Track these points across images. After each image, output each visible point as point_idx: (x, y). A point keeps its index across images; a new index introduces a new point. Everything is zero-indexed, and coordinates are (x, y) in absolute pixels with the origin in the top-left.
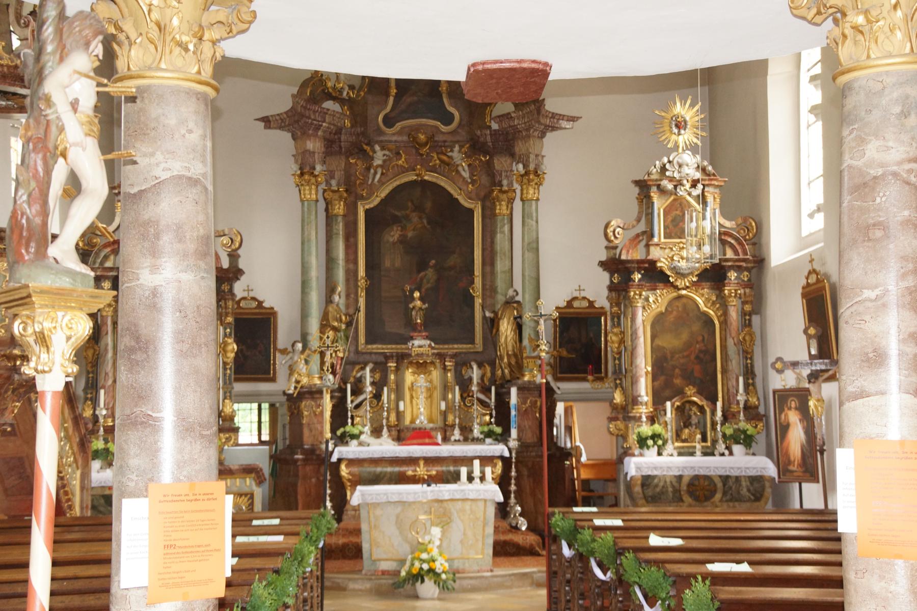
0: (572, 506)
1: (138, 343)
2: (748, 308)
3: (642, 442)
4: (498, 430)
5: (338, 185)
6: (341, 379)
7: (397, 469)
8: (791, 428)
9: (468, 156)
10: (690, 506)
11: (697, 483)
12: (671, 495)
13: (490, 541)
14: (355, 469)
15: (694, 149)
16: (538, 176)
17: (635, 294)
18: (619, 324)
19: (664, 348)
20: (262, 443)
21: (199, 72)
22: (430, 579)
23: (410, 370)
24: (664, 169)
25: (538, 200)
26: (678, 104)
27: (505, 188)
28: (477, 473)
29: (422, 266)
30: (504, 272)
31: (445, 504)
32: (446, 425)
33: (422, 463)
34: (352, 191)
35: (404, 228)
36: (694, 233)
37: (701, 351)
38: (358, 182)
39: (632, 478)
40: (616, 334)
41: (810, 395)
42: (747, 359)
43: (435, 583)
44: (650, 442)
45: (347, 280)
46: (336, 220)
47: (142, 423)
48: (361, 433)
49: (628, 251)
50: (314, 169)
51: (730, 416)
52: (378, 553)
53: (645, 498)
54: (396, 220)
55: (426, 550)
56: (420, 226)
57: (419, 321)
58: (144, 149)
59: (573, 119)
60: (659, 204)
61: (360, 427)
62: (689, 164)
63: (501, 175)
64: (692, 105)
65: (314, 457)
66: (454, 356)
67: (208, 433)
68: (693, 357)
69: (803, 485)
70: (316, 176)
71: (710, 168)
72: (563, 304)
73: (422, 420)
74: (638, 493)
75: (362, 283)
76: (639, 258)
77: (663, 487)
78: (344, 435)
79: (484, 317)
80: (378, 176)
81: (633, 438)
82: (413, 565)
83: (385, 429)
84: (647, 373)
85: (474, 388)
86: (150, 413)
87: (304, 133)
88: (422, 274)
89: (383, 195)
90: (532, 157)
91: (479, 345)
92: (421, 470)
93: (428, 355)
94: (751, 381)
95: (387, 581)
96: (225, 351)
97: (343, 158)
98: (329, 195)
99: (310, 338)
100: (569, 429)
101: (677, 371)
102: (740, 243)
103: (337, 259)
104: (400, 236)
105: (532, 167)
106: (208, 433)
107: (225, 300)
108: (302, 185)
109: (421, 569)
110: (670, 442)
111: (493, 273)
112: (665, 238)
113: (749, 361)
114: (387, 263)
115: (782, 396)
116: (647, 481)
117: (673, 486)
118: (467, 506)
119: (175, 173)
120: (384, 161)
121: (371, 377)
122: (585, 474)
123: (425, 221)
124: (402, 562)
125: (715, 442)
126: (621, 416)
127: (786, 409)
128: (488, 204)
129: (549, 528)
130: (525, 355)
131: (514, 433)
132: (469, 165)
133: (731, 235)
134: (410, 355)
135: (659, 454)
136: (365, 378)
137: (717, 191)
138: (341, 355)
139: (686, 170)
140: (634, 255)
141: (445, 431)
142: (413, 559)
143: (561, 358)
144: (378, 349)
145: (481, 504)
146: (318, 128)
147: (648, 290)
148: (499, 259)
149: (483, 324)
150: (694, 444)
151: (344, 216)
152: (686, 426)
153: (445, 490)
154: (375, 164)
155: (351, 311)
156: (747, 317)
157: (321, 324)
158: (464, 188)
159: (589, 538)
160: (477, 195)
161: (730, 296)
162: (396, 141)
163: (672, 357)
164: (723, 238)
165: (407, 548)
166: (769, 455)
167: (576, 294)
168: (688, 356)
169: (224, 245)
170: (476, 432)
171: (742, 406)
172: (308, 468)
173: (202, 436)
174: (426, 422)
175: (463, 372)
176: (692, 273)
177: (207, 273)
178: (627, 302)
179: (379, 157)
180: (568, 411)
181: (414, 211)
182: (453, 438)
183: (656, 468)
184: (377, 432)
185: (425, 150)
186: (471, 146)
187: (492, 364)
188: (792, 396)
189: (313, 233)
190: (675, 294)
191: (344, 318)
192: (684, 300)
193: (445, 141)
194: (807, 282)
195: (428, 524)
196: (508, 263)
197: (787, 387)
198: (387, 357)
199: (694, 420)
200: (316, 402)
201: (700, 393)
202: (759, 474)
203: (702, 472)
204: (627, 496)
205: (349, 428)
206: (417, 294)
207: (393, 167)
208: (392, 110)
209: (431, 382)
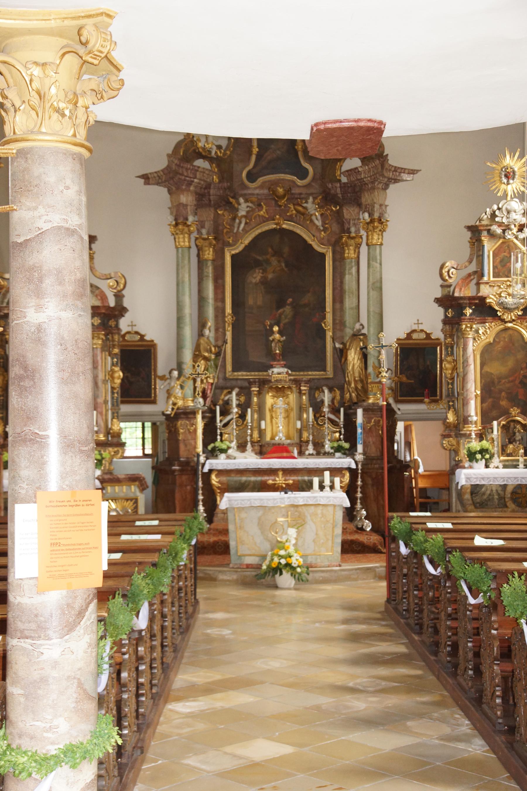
1: (26, 372)
3: (472, 456)
4: (347, 445)
5: (208, 234)
6: (212, 401)
7: (259, 478)
9: (321, 207)
10: (513, 511)
11: (519, 491)
13: (339, 540)
14: (224, 479)
16: (382, 223)
17: (467, 327)
18: (452, 354)
19: (492, 374)
20: (145, 456)
21: (74, 135)
22: (288, 572)
23: (270, 394)
24: (493, 215)
25: (381, 244)
27: (353, 235)
28: (327, 482)
29: (280, 304)
30: (352, 308)
31: (300, 509)
32: (301, 441)
33: (280, 473)
34: (220, 238)
35: (264, 271)
38: (225, 231)
39: (462, 486)
40: (449, 362)
43: (292, 575)
45: (216, 317)
46: (207, 264)
47: (31, 440)
48: (229, 448)
49: (461, 289)
50: (187, 219)
52: (243, 550)
53: (474, 504)
54: (258, 264)
55: (283, 548)
56: (279, 268)
57: (278, 352)
58: (28, 204)
59: (413, 172)
60: (489, 247)
61: (227, 443)
63: (349, 223)
65: (189, 468)
66: (308, 382)
67: (86, 448)
68: (517, 382)
70: (189, 226)
72: (403, 336)
73: (281, 437)
74: (468, 500)
75: (229, 319)
76: (470, 295)
77: (490, 495)
78: (214, 450)
79: (335, 348)
80: (242, 226)
81: (463, 452)
82: (272, 560)
83: (249, 445)
84: (476, 396)
85: (326, 410)
86: (37, 431)
87: (178, 189)
88: (281, 311)
89: (247, 242)
90: (377, 207)
91: (330, 372)
92: (280, 480)
93: (285, 381)
95: (251, 573)
96: (113, 377)
97: (212, 210)
98: (200, 243)
99: (184, 366)
100: (408, 444)
103: (208, 298)
104: (262, 277)
105: (376, 216)
106: (86, 448)
107: (112, 334)
108: (177, 234)
109: (280, 563)
110: (496, 456)
111: (342, 309)
112: (494, 277)
114: (251, 301)
116: (475, 489)
117: (499, 494)
118: (319, 510)
119: (55, 224)
120: (248, 212)
121: (237, 400)
122: (422, 484)
123: (283, 265)
124: (264, 557)
126: (453, 434)
128: (338, 249)
129: (389, 529)
130: (369, 381)
131: (360, 448)
132: (322, 215)
134: (270, 381)
135: (487, 466)
136: (232, 401)
138: (211, 381)
139: (513, 216)
141: (301, 447)
142: (273, 555)
143: (401, 384)
144: (243, 376)
145: (331, 509)
146: (190, 183)
147: (478, 323)
148: (347, 297)
149: (334, 354)
150: (517, 458)
151: (213, 260)
152: (510, 442)
153: (300, 497)
154: (240, 215)
155: (220, 343)
157: (194, 354)
158: (317, 234)
160: (328, 240)
162: (258, 194)
163: (499, 382)
165: (268, 546)
167: (415, 327)
169: (111, 287)
170: (327, 447)
172: (184, 478)
173: (81, 451)
174: (284, 439)
175: (316, 395)
176: (517, 308)
177: (84, 311)
178: (459, 334)
179: (243, 208)
180: (407, 429)
181: (273, 256)
182: (307, 453)
184: (242, 447)
185: (283, 202)
186: (323, 197)
187: (341, 389)
189: (187, 276)
190: (502, 327)
191: (213, 349)
192: (511, 332)
193: (301, 194)
195: (286, 526)
196: (355, 301)
198: (251, 383)
200: (190, 421)
204: (458, 502)
205: (218, 444)
206: (276, 329)
207: (255, 217)
208: (254, 167)
209: (288, 404)
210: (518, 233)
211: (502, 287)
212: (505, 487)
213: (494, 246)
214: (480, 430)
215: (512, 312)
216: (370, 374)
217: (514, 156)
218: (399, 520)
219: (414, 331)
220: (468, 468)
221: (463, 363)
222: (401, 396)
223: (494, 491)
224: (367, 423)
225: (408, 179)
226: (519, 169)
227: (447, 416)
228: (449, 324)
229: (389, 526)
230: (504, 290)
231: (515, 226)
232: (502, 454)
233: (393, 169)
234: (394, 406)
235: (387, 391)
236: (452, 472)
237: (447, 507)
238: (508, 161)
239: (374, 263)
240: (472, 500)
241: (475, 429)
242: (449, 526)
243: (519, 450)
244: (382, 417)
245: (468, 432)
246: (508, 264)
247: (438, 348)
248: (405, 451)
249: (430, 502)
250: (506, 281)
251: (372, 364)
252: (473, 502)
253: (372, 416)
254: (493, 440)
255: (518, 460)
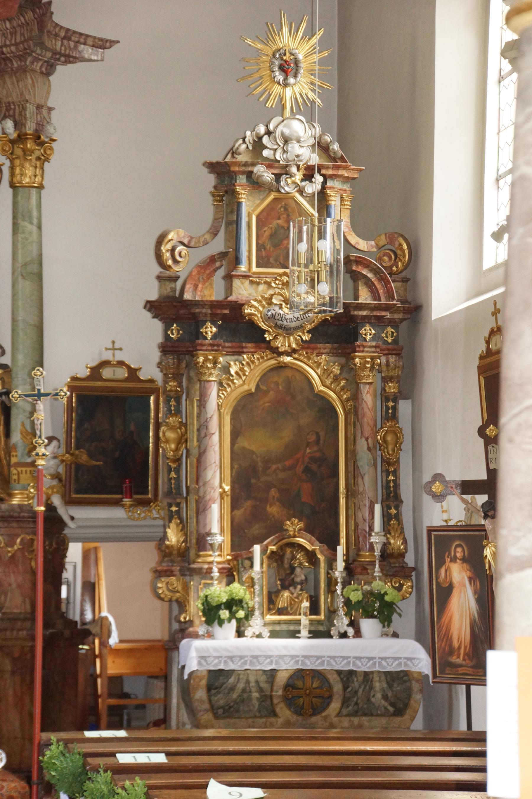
0: (83, 728)
2: (392, 388)
3: (211, 613)
8: (455, 593)
10: (288, 724)
11: (299, 684)
12: (256, 703)
15: (306, 110)
17: (206, 360)
18: (178, 412)
19: (252, 452)
24: (258, 145)
25: (41, 187)
26: (286, 30)
36: (302, 261)
37: (313, 459)
39: (191, 674)
40: (172, 428)
41: (486, 537)
42: (388, 473)
44: (224, 614)
49: (196, 287)
51: (359, 570)
53: (213, 709)
59: (103, 44)
60: (250, 206)
62: (301, 138)
64: (310, 33)
68: (299, 469)
69: (473, 688)
71: (336, 147)
74: (202, 701)
76: (213, 298)
77: (244, 690)
81: (195, 606)
84: (222, 496)
90: (31, 109)
94: (393, 511)
100: (90, 588)
101: (273, 492)
102: (382, 279)
105: (30, 127)
110: (257, 613)
112: (258, 266)
113: (391, 478)
115: (442, 539)
116: (217, 679)
117: (261, 690)
122: (114, 667)
125: (332, 612)
126: (176, 569)
127: (448, 560)
129: (40, 769)
130: (14, 460)
133: (367, 265)
135: (240, 634)
137: (347, 187)
139: (295, 148)
140: (206, 292)
143: (78, 467)
147: (228, 354)
150: (297, 617)
152: (285, 587)
156: (391, 404)
159: (105, 789)
161: (363, 367)
163: (266, 468)
164: (351, 266)
166: (419, 638)
167: (108, 356)
168: (292, 468)
171: (377, 553)
176: (300, 328)
178: (192, 374)
180: (88, 557)
183: (231, 658)
188: (460, 538)
190: (273, 362)
192: (288, 373)
194: (488, 348)
197: (451, 523)
199: (300, 575)
201: (309, 529)
202: (403, 668)
203: (309, 665)
204: (182, 706)
210: (304, 183)
211: (273, 285)
212: (273, 673)
213: (259, 205)
214: (228, 561)
215: (291, 334)
216: (15, 447)
217: (297, 31)
218: (61, 748)
219: (105, 364)
220: (203, 637)
221: (198, 430)
222: (77, 492)
223: (253, 684)
224: (7, 545)
225: (94, 57)
226: (306, 56)
227: (165, 533)
228: (172, 352)
229: (40, 762)
230: (277, 291)
231: (298, 169)
232: (269, 609)
233: (62, 34)
234: (63, 511)
235: (47, 482)
236: (170, 647)
237: (162, 716)
238: (286, 39)
239: (26, 224)
240: (210, 701)
241: (219, 559)
242: (160, 758)
243: (302, 602)
244: (35, 533)
245: (206, 566)
246: (285, 242)
247: (152, 398)
248: (83, 601)
249: (123, 711)
250: (281, 275)
251: (19, 427)
252: (212, 706)
253: (18, 531)
254: (252, 583)
255: (298, 622)
